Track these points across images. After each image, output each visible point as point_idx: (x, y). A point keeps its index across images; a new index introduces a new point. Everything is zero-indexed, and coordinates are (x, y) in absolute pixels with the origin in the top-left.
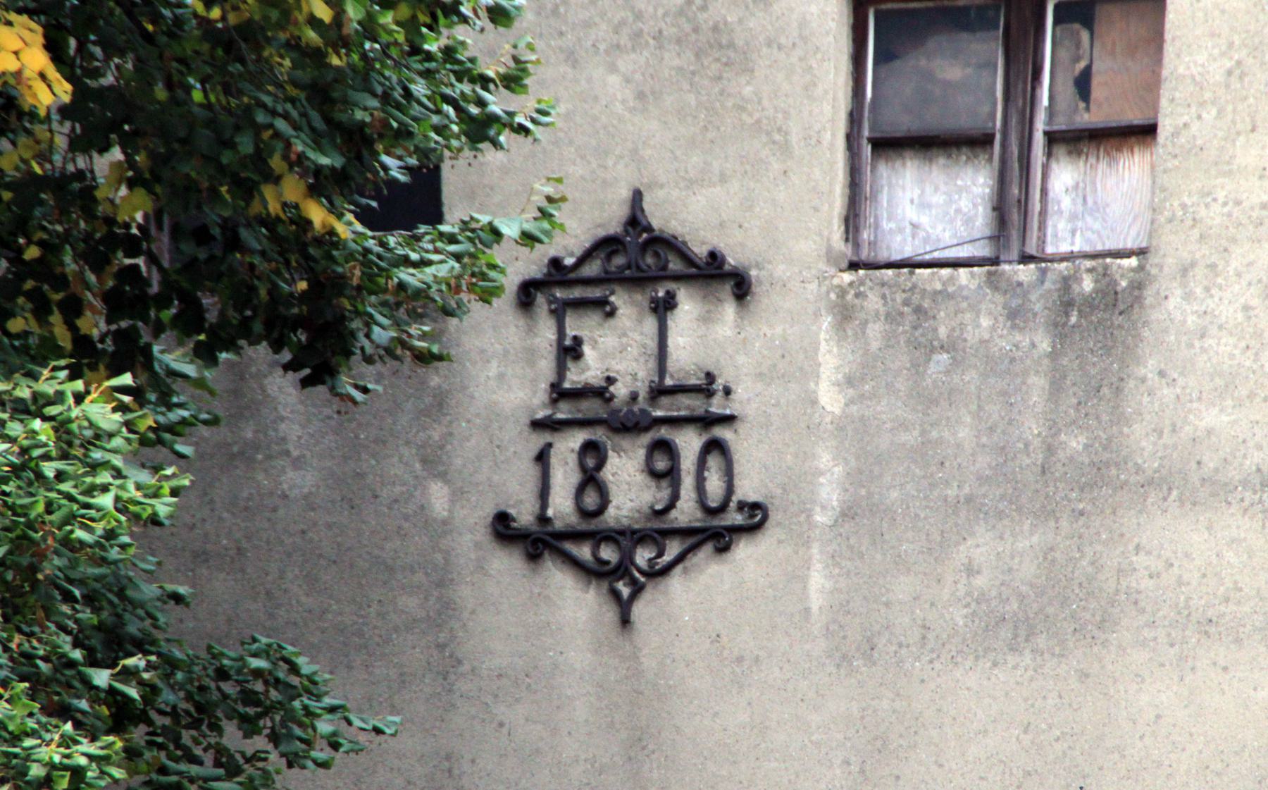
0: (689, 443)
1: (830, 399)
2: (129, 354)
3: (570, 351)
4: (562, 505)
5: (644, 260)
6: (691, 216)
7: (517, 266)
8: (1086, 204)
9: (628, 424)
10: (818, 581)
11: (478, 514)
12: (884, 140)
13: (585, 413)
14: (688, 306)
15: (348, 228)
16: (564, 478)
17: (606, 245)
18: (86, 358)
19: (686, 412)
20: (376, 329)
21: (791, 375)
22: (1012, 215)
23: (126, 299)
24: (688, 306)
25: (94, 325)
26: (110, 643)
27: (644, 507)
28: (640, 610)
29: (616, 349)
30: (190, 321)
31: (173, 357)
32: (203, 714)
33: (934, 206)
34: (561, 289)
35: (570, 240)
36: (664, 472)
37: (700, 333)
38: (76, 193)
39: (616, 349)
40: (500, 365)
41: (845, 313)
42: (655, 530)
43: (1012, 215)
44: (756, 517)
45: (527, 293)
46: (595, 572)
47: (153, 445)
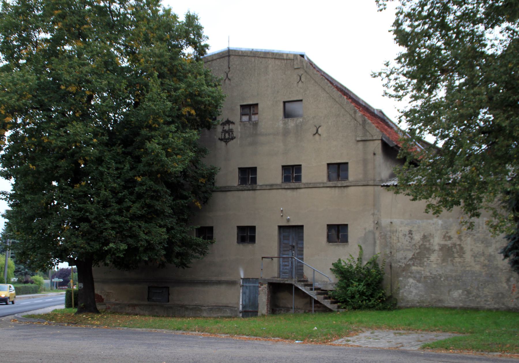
0: (231, 133)
1: (239, 130)
2: (198, 129)
3: (224, 128)
4: (223, 137)
5: (228, 122)
6: (231, 119)
7: (221, 123)
8: (254, 118)
9: (227, 132)
10: (239, 142)
11: (217, 138)
12: (242, 114)
13: (225, 131)
14: (231, 125)
15: (211, 121)
16: (223, 135)
17: (226, 121)
18: (195, 129)
19: (230, 131)
20: (445, 51)
21: (237, 129)
22: (250, 119)
23: (198, 126)
24: (231, 125)
25: (196, 127)
26: (194, 147)
27: (228, 137)
28: (228, 144)
29: (226, 128)
30: (201, 127)
31: (200, 129)
32: (200, 152)
33: (245, 118)
34: (223, 124)
35: (224, 121)
36: (229, 135)
37: (231, 126)
38: (195, 119)
39: (226, 128)
40: (219, 129)
41: (240, 125)
42: (229, 139)
43: (250, 119)
44: (235, 138)
45: (221, 124)
46: (225, 142)
47: (198, 134)
